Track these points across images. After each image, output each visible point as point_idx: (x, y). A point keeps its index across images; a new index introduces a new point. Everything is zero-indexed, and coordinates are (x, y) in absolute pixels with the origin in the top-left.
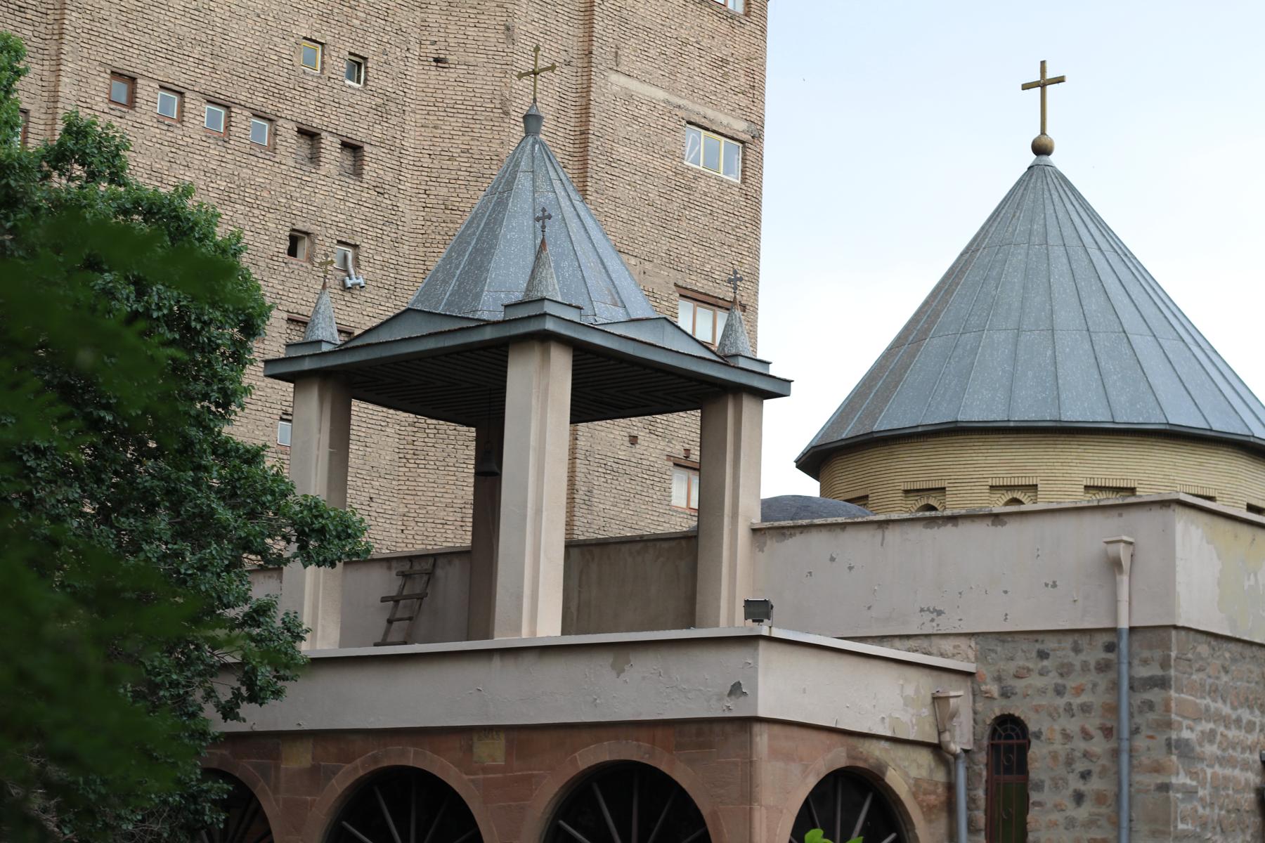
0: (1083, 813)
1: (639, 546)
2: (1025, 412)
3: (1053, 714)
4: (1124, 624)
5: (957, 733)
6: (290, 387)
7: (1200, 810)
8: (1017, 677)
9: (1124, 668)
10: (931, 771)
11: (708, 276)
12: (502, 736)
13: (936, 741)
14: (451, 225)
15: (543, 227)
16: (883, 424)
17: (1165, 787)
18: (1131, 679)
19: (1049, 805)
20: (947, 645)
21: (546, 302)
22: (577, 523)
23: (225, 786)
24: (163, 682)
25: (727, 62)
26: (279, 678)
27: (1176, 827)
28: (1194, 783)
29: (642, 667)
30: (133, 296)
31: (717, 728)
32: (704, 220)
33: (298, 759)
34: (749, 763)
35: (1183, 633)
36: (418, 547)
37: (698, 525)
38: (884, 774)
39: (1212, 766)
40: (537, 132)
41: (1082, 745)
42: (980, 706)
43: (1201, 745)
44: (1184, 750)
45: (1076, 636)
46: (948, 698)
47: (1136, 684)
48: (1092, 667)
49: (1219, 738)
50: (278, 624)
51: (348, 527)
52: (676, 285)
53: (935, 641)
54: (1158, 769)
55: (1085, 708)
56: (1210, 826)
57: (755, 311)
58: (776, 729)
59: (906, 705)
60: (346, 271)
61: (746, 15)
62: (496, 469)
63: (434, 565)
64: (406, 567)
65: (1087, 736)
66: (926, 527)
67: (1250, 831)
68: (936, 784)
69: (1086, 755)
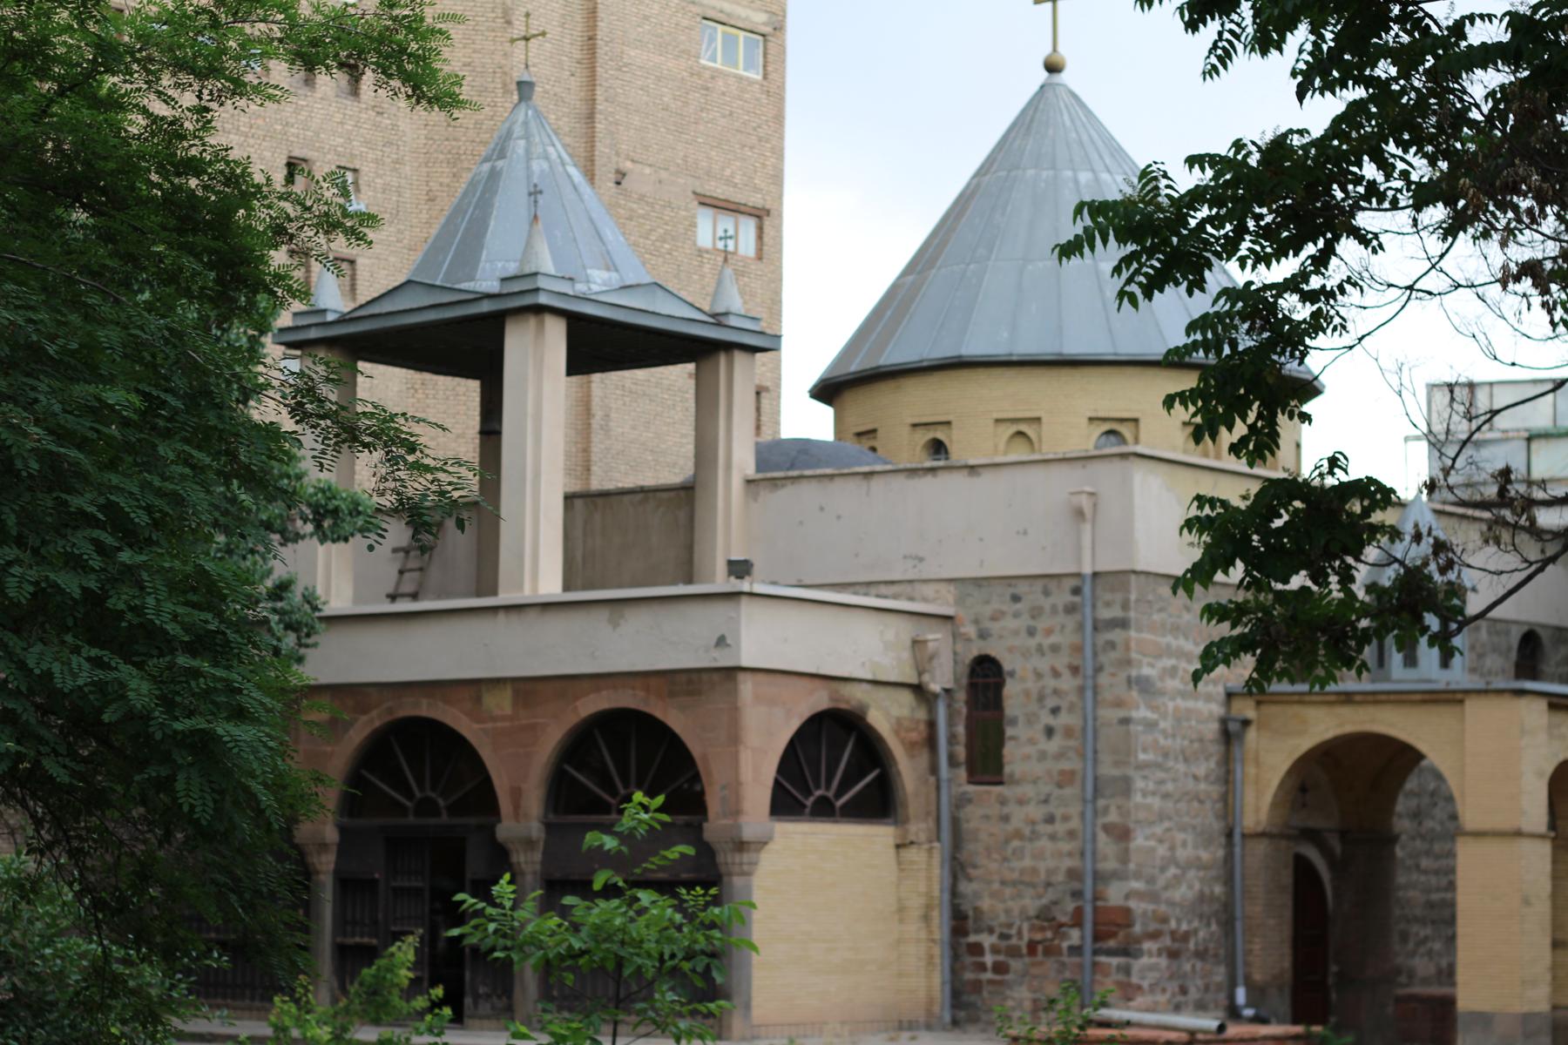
0: (1053, 746)
1: (639, 497)
2: (1028, 346)
3: (1026, 654)
4: (1087, 570)
7: (1162, 741)
8: (994, 618)
9: (1088, 610)
11: (729, 182)
14: (454, 143)
15: (536, 202)
16: (893, 356)
17: (1126, 721)
20: (928, 590)
26: (300, 645)
27: (1136, 757)
29: (636, 621)
31: (705, 677)
32: (723, 122)
34: (734, 712)
35: (1142, 577)
37: (695, 475)
39: (1173, 699)
40: (530, 98)
41: (1050, 683)
42: (960, 647)
44: (1145, 686)
45: (1046, 581)
48: (1060, 608)
49: (1181, 673)
51: (359, 504)
52: (695, 193)
53: (917, 586)
54: (1119, 704)
55: (1055, 649)
57: (780, 216)
58: (760, 677)
62: (497, 427)
65: (1056, 674)
68: (918, 722)
69: (1056, 692)
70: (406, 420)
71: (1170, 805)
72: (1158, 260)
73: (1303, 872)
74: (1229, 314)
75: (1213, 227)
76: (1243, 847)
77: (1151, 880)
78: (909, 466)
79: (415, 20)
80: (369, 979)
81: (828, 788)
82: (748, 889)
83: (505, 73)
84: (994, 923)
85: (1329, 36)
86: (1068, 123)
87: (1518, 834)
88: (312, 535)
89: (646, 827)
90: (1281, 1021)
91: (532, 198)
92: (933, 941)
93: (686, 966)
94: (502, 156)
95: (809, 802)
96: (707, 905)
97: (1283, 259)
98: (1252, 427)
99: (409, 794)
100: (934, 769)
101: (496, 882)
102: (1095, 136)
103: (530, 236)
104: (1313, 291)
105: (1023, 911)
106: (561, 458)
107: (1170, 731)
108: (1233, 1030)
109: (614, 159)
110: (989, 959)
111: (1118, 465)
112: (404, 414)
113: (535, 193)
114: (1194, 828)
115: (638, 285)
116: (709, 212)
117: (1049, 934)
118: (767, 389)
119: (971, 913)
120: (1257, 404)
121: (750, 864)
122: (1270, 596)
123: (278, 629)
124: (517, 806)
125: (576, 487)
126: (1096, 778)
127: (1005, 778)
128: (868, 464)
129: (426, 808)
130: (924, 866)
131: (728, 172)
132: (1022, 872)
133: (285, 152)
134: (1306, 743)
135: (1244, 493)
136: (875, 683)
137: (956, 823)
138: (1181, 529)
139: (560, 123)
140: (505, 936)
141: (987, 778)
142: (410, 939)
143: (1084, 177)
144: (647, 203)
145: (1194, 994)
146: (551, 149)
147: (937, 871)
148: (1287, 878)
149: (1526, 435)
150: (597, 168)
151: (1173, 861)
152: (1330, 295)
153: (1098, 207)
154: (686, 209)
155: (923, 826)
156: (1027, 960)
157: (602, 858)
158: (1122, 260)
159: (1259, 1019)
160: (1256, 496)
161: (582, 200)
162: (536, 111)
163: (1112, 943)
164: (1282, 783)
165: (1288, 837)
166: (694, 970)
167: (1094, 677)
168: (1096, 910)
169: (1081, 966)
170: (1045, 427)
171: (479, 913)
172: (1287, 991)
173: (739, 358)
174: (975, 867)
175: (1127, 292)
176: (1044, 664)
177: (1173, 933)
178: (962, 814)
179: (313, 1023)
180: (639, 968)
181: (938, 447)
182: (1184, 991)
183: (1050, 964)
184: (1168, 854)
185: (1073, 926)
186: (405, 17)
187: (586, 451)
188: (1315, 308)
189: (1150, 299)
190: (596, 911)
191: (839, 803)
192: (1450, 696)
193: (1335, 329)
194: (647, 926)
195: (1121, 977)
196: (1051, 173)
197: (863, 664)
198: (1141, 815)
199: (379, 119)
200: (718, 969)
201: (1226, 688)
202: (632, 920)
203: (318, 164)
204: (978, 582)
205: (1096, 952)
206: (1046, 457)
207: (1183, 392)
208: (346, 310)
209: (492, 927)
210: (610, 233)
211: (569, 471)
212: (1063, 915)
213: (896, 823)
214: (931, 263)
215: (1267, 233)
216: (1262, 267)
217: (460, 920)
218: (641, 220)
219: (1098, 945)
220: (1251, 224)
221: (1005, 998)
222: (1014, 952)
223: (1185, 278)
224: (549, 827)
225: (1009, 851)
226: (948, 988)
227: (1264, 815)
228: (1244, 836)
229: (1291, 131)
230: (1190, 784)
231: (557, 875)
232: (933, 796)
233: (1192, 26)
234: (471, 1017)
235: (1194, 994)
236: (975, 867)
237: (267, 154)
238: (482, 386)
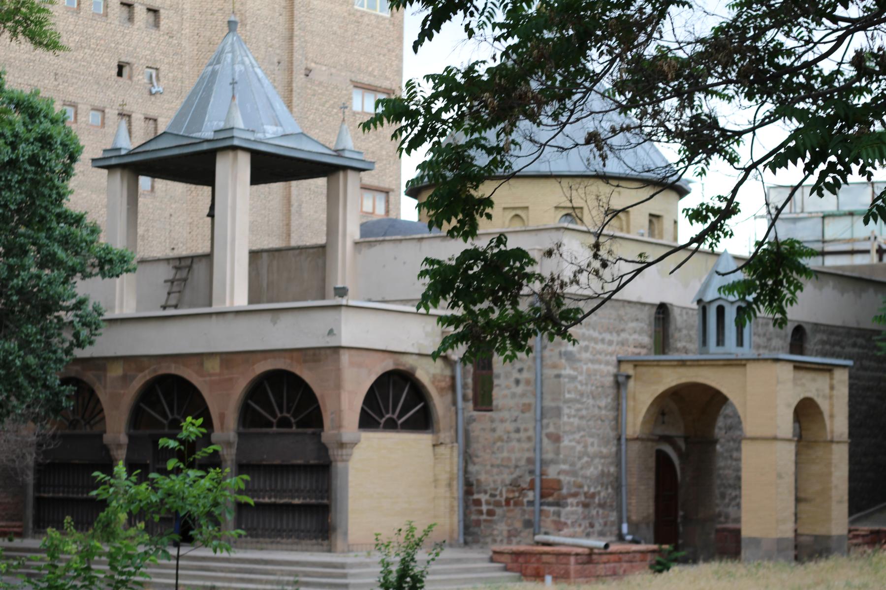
0: (519, 390)
1: (297, 252)
6: (105, 171)
7: (579, 387)
11: (371, 74)
17: (558, 376)
23: (73, 388)
24: (33, 340)
26: (92, 335)
27: (564, 396)
29: (286, 320)
30: (10, 151)
31: (323, 352)
32: (367, 41)
33: (115, 372)
34: (338, 371)
36: (184, 253)
39: (586, 364)
49: (591, 349)
52: (351, 81)
54: (555, 366)
58: (353, 352)
60: (151, 83)
63: (192, 262)
64: (177, 263)
68: (445, 377)
71: (584, 422)
73: (662, 461)
76: (626, 446)
77: (573, 464)
80: (103, 519)
81: (394, 412)
82: (346, 470)
83: (242, 14)
84: (488, 488)
87: (775, 439)
90: (647, 542)
92: (453, 498)
94: (218, 62)
95: (383, 421)
100: (454, 403)
103: (230, 107)
105: (503, 481)
107: (584, 382)
109: (304, 62)
110: (484, 508)
114: (598, 435)
115: (291, 134)
116: (360, 91)
117: (517, 494)
118: (393, 190)
119: (475, 482)
121: (347, 455)
123: (78, 326)
126: (542, 408)
127: (494, 408)
130: (448, 456)
131: (370, 69)
132: (502, 460)
133: (117, 59)
134: (661, 389)
135: (451, 257)
136: (420, 355)
137: (467, 433)
139: (274, 42)
141: (484, 408)
144: (324, 87)
145: (598, 527)
146: (246, 59)
147: (455, 459)
148: (652, 463)
149: (822, 215)
150: (294, 67)
151: (585, 453)
154: (346, 90)
155: (448, 434)
156: (505, 508)
157: (169, 453)
159: (635, 542)
161: (263, 87)
162: (238, 37)
163: (550, 499)
164: (648, 410)
168: (542, 481)
169: (534, 512)
172: (652, 526)
173: (351, 174)
174: (477, 457)
177: (585, 494)
178: (470, 428)
182: (592, 525)
183: (518, 511)
184: (583, 449)
185: (529, 489)
187: (288, 225)
191: (400, 422)
192: (739, 362)
195: (555, 518)
197: (413, 345)
198: (567, 428)
199: (170, 40)
201: (617, 358)
203: (136, 65)
205: (542, 504)
206: (528, 228)
208: (132, 147)
212: (524, 484)
213: (433, 432)
218: (320, 96)
219: (543, 500)
221: (493, 530)
222: (498, 504)
224: (240, 435)
226: (462, 524)
227: (638, 428)
228: (627, 440)
230: (596, 411)
231: (244, 461)
232: (454, 417)
235: (598, 527)
236: (477, 457)
237: (107, 60)
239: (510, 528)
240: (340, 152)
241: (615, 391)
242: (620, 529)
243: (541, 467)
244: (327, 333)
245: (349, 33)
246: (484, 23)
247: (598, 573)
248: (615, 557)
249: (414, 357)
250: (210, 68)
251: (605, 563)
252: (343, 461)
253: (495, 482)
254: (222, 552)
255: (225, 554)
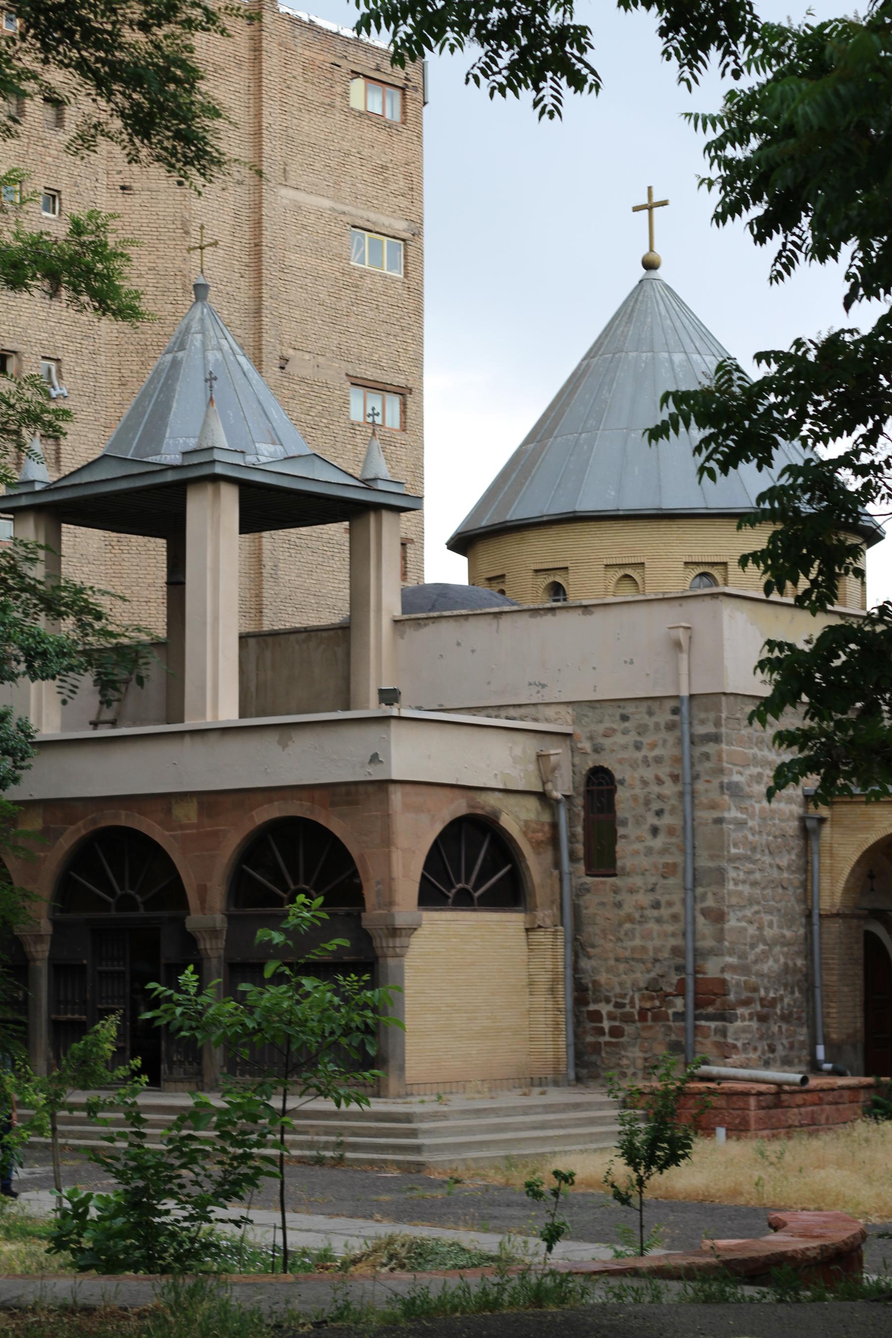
0: (658, 843)
1: (304, 635)
3: (634, 765)
4: (685, 693)
5: (559, 782)
7: (750, 837)
8: (606, 736)
9: (686, 727)
10: (538, 814)
11: (377, 365)
12: (195, 800)
13: (541, 790)
14: (142, 336)
15: (211, 387)
16: (517, 513)
17: (719, 821)
18: (692, 736)
19: (632, 837)
20: (550, 712)
21: (215, 450)
22: (265, 595)
25: (387, 168)
26: (16, 767)
27: (729, 851)
28: (744, 816)
29: (303, 742)
31: (361, 789)
32: (371, 314)
34: (387, 817)
35: (732, 698)
37: (350, 617)
38: (498, 818)
39: (759, 802)
40: (205, 298)
41: (655, 789)
42: (577, 760)
43: (749, 786)
44: (734, 790)
45: (650, 702)
46: (549, 755)
47: (696, 740)
50: (13, 728)
52: (347, 375)
54: (713, 806)
55: (658, 760)
56: (759, 850)
58: (408, 788)
59: (515, 762)
61: (404, 123)
65: (659, 781)
66: (531, 616)
67: (795, 852)
68: (543, 824)
69: (660, 797)
70: (94, 592)
72: (733, 440)
73: (872, 944)
74: (791, 486)
75: (779, 412)
77: (743, 956)
78: (532, 607)
79: (100, 245)
81: (467, 882)
82: (401, 968)
83: (184, 276)
85: (876, 245)
86: (663, 312)
88: (24, 674)
89: (308, 924)
91: (208, 384)
92: (559, 1010)
93: (344, 1041)
94: (182, 348)
95: (451, 895)
96: (362, 988)
97: (839, 438)
98: (814, 582)
99: (112, 893)
101: (182, 973)
102: (686, 322)
103: (207, 416)
104: (863, 466)
106: (236, 598)
108: (814, 1082)
109: (279, 347)
110: (606, 1025)
111: (709, 603)
112: (91, 588)
113: (211, 379)
114: (779, 910)
116: (361, 391)
118: (412, 541)
119: (590, 985)
120: (817, 562)
122: (832, 724)
124: (203, 901)
125: (251, 628)
126: (694, 869)
128: (498, 605)
129: (126, 903)
132: (633, 950)
134: (873, 838)
135: (807, 638)
138: (755, 669)
140: (190, 1018)
141: (602, 871)
142: (112, 1018)
143: (678, 358)
145: (781, 1052)
146: (224, 342)
148: (859, 951)
150: (264, 355)
151: (762, 939)
152: (878, 469)
153: (681, 397)
156: (639, 1025)
158: (702, 441)
159: (837, 1072)
160: (818, 640)
163: (710, 1010)
164: (853, 871)
165: (858, 917)
166: (350, 1045)
167: (692, 784)
168: (696, 981)
169: (685, 1029)
170: (647, 571)
171: (169, 999)
172: (860, 1046)
173: (387, 517)
174: (593, 946)
175: (706, 468)
176: (649, 774)
179: (31, 1090)
180: (304, 1043)
181: (557, 590)
183: (659, 1029)
186: (91, 242)
187: (259, 596)
188: (866, 479)
189: (726, 474)
190: (267, 995)
191: (477, 894)
193: (882, 498)
194: (310, 1008)
195: (719, 1039)
196: (649, 354)
198: (734, 900)
200: (371, 1044)
202: (298, 1002)
204: (593, 704)
205: (697, 1018)
207: (756, 552)
209: (179, 1010)
210: (276, 413)
211: (243, 614)
213: (525, 911)
214: (549, 433)
215: (823, 416)
216: (820, 446)
217: (155, 1004)
219: (698, 1012)
220: (811, 409)
222: (627, 1018)
223: (755, 456)
224: (230, 918)
225: (622, 933)
226: (572, 1050)
228: (821, 916)
229: (843, 331)
230: (775, 873)
231: (239, 959)
232: (557, 886)
233: (760, 239)
234: (166, 1081)
235: (781, 1052)
236: (593, 946)
238: (168, 544)
239: (647, 1055)
240: (370, 483)
241: (801, 843)
242: (813, 1053)
243: (695, 960)
244: (369, 758)
245: (343, 304)
246: (779, 273)
247: (790, 1122)
248: (814, 1097)
249: (497, 794)
250: (169, 357)
251: (799, 1106)
252: (397, 956)
253: (621, 984)
254: (348, 1105)
255: (354, 1107)
